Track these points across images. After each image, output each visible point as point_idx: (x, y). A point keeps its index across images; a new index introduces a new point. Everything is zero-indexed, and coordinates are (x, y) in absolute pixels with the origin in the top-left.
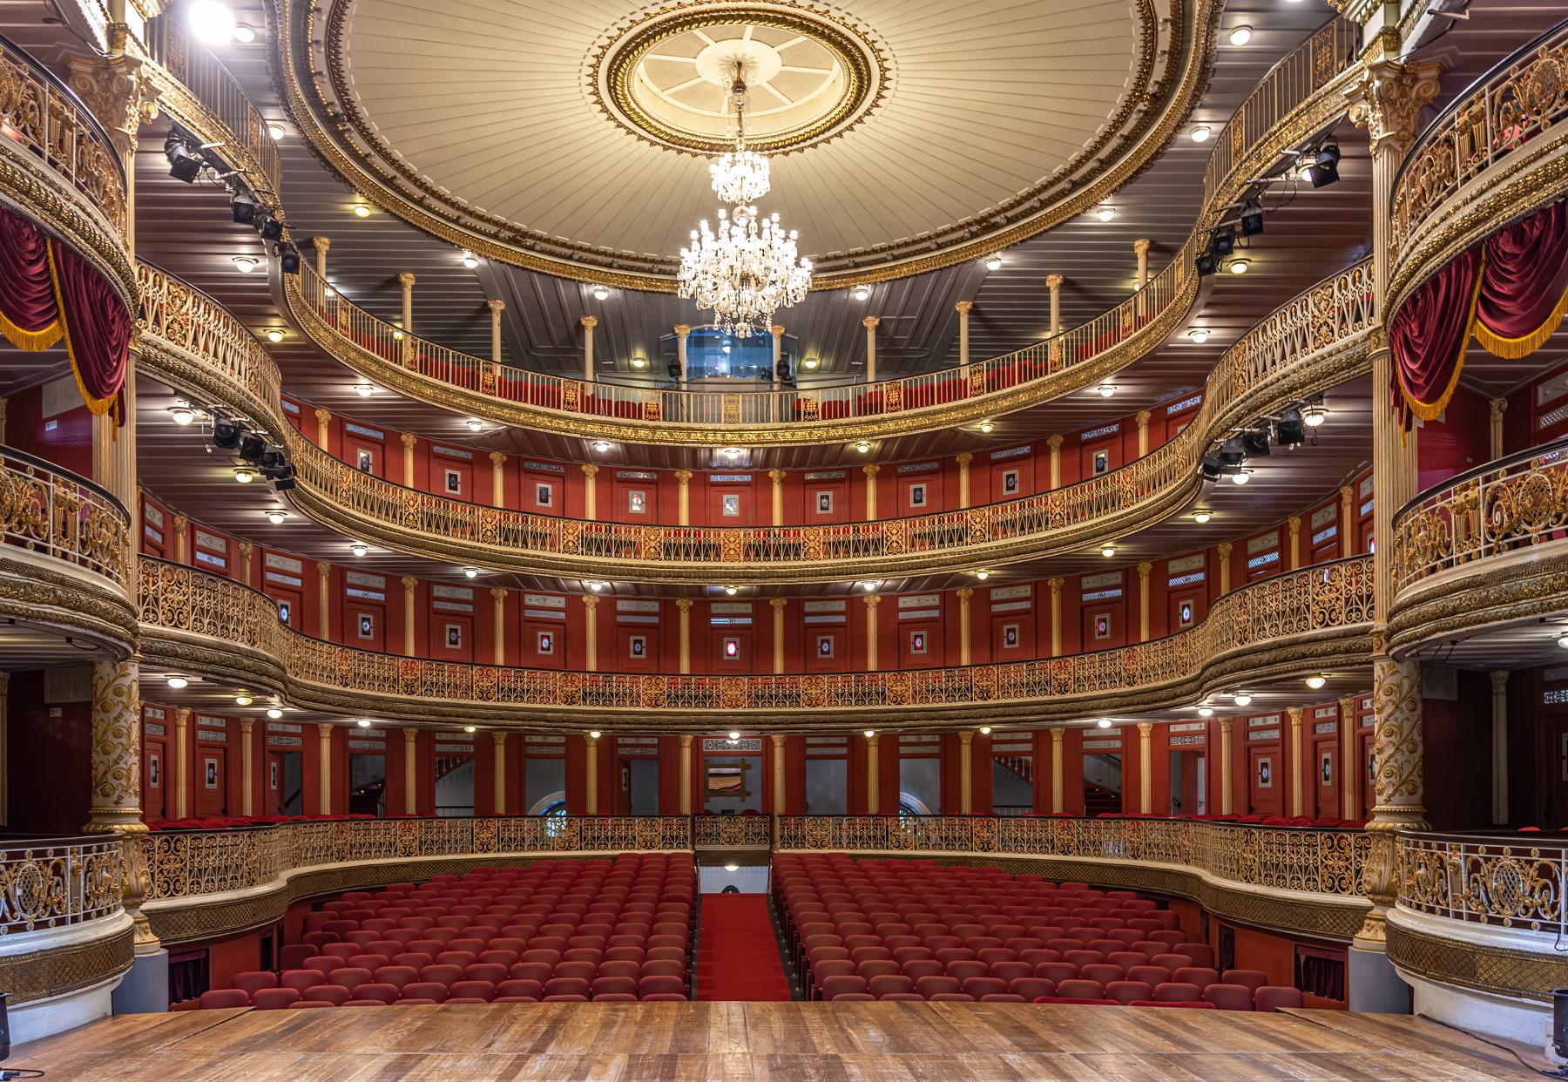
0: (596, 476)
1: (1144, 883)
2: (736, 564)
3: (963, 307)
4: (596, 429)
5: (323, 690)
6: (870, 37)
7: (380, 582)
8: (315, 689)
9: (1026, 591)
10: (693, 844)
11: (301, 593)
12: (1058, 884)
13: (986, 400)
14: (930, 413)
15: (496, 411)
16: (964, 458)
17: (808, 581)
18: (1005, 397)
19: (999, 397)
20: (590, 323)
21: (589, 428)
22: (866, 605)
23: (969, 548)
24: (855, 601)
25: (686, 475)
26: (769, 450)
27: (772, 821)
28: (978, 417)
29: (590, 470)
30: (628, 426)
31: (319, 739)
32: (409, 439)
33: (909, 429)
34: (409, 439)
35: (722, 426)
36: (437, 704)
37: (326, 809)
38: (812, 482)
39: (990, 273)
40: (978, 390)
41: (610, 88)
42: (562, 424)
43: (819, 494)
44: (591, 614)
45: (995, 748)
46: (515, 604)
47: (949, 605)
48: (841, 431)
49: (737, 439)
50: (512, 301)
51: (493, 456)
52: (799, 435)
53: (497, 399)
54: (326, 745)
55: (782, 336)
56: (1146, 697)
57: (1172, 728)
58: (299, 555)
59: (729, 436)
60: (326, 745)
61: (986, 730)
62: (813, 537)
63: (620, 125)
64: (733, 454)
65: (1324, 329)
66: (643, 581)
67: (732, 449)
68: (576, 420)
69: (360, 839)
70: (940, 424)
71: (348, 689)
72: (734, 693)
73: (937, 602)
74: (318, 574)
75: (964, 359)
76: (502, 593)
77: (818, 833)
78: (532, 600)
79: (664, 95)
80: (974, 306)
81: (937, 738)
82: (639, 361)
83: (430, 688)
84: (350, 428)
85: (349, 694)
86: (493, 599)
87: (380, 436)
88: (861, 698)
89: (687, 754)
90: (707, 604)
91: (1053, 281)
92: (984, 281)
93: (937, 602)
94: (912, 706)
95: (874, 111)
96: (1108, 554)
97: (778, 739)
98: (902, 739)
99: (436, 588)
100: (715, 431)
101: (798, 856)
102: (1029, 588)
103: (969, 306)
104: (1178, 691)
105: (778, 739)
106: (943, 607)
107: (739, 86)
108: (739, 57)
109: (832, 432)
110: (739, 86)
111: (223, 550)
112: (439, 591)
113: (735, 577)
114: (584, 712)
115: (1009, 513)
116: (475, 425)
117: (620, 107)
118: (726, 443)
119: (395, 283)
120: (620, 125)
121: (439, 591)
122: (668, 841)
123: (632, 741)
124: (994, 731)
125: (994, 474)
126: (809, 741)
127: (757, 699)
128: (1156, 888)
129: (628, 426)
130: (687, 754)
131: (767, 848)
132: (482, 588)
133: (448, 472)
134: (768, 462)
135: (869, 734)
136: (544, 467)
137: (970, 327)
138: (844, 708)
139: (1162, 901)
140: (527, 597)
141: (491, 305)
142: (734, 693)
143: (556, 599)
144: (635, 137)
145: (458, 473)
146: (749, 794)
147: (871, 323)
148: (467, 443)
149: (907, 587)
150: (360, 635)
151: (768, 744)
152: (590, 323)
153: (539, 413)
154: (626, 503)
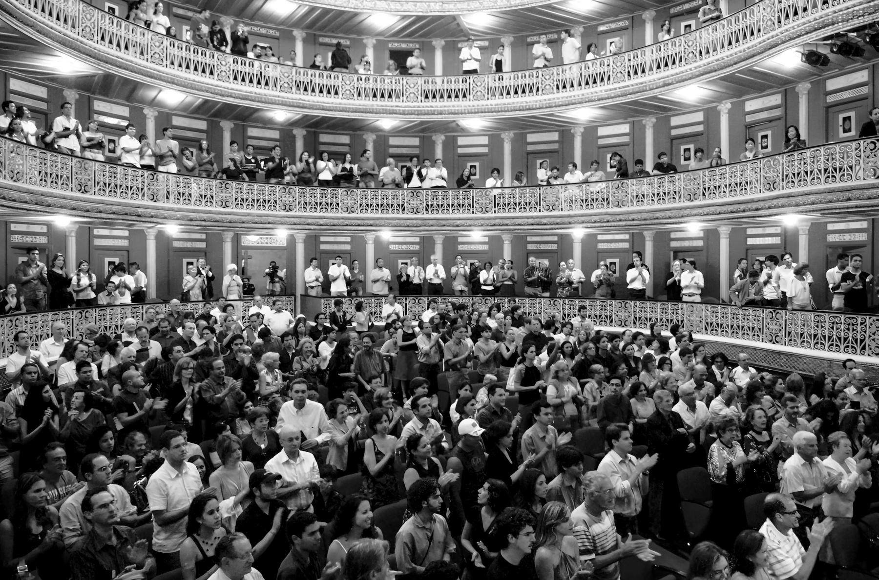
9: (625, 128)
94: (166, 205)
102: (702, 113)
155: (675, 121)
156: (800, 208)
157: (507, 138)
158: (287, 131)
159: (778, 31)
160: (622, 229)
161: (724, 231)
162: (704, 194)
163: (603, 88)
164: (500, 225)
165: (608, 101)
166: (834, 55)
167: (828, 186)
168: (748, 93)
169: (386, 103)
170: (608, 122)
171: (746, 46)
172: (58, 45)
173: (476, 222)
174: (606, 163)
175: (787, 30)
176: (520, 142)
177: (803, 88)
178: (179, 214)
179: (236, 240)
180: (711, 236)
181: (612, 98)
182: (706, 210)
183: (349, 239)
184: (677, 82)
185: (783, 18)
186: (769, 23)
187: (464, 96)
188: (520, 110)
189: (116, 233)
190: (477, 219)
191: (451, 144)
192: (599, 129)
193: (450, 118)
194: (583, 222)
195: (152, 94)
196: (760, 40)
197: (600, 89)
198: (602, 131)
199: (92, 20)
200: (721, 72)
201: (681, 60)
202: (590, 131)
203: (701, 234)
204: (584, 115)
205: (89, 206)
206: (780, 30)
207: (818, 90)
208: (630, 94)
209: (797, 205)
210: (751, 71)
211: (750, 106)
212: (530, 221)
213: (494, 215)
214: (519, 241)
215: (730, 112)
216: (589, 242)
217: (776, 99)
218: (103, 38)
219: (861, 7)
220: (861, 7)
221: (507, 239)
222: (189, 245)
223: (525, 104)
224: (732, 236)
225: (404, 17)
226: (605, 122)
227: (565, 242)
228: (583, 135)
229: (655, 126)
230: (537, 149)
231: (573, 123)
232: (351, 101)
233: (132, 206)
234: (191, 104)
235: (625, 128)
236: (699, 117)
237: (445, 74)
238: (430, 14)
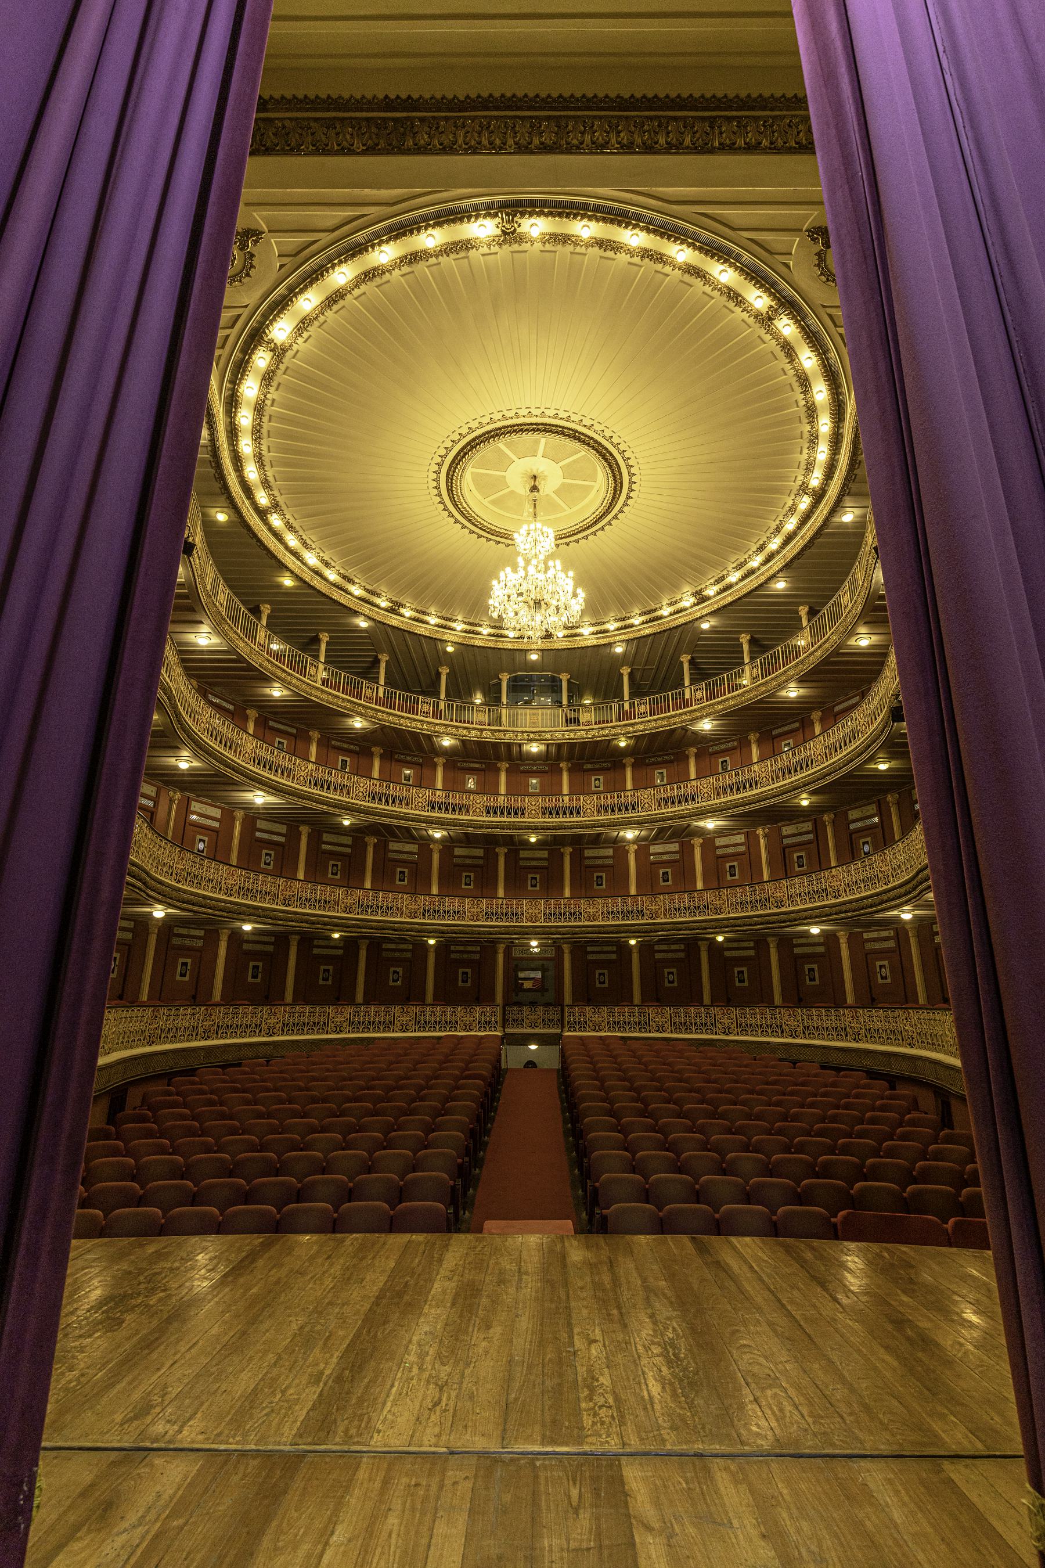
0: (444, 765)
1: (868, 1063)
2: (536, 820)
3: (685, 659)
4: (442, 729)
5: (204, 897)
6: (622, 447)
7: (283, 829)
8: (192, 894)
9: (741, 839)
10: (504, 1027)
11: (217, 832)
12: (794, 1063)
13: (706, 706)
14: (667, 717)
15: (371, 713)
17: (587, 831)
18: (719, 703)
19: (715, 704)
20: (444, 671)
21: (437, 728)
22: (627, 852)
24: (619, 844)
25: (504, 765)
26: (559, 746)
27: (563, 1011)
28: (701, 718)
29: (440, 761)
30: (464, 728)
31: (218, 940)
32: (315, 735)
33: (654, 728)
34: (315, 735)
35: (528, 729)
36: (308, 915)
37: (144, 997)
39: (703, 632)
40: (699, 701)
41: (448, 490)
42: (419, 725)
43: (593, 778)
44: (436, 857)
45: (727, 954)
46: (381, 848)
47: (686, 850)
48: (607, 732)
49: (537, 737)
50: (393, 653)
51: (373, 749)
52: (579, 735)
53: (374, 706)
54: (223, 947)
55: (569, 681)
56: (853, 906)
57: (865, 936)
58: (219, 804)
59: (532, 736)
60: (223, 947)
61: (720, 939)
62: (588, 802)
63: (457, 521)
64: (534, 748)
66: (471, 831)
67: (534, 744)
68: (428, 723)
69: (228, 1021)
70: (675, 723)
71: (232, 899)
72: (596, 1019)
73: (677, 849)
74: (233, 819)
75: (687, 682)
76: (371, 840)
77: (596, 1019)
78: (394, 846)
79: (485, 502)
80: (692, 658)
81: (682, 947)
82: (478, 699)
83: (305, 901)
84: (271, 723)
85: (231, 902)
86: (366, 845)
87: (295, 731)
88: (625, 915)
89: (500, 958)
90: (517, 851)
91: (744, 639)
92: (699, 639)
93: (677, 849)
95: (625, 509)
96: (805, 803)
97: (566, 948)
98: (656, 947)
99: (325, 835)
100: (522, 732)
101: (581, 1038)
103: (689, 657)
104: (885, 897)
105: (566, 948)
106: (682, 851)
107: (534, 489)
108: (535, 473)
109: (602, 732)
110: (534, 489)
111: (153, 794)
112: (326, 837)
113: (534, 828)
114: (422, 924)
115: (727, 779)
116: (358, 723)
117: (455, 505)
118: (531, 740)
119: (316, 640)
120: (457, 521)
121: (326, 837)
122: (483, 1025)
123: (461, 948)
124: (726, 940)
125: (713, 760)
126: (589, 949)
127: (548, 916)
128: (882, 1069)
129: (464, 728)
130: (500, 958)
131: (559, 1031)
132: (358, 832)
133: (341, 758)
134: (559, 757)
135: (633, 942)
136: (409, 758)
137: (691, 674)
138: (613, 923)
139: (893, 1081)
140: (391, 844)
141: (380, 657)
143: (412, 846)
144: (467, 531)
145: (348, 759)
146: (547, 990)
147: (625, 671)
148: (352, 739)
149: (656, 837)
150: (206, 839)
151: (559, 950)
152: (444, 671)
153: (403, 717)
154: (464, 783)
211: (787, 830)
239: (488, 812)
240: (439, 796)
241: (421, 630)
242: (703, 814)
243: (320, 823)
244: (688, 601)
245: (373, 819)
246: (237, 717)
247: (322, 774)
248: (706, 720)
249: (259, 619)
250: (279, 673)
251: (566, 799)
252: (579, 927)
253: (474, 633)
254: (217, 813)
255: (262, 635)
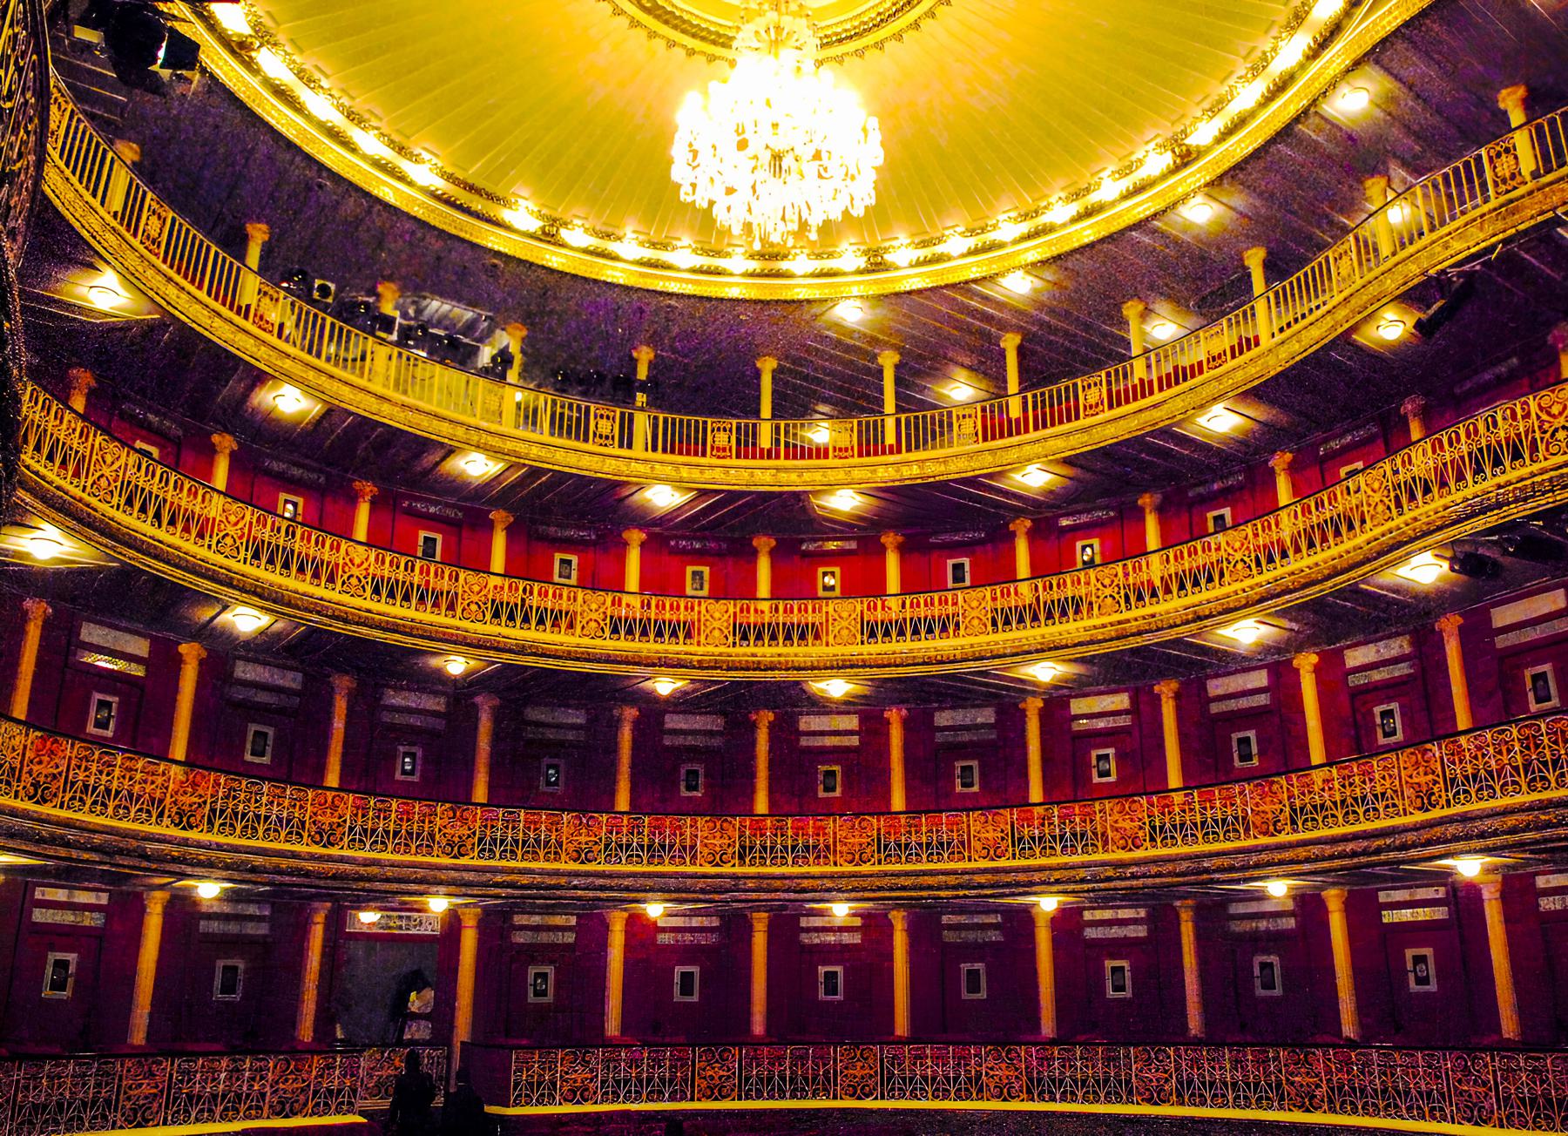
16: (1022, 526)
23: (831, 650)
29: (635, 537)
38: (684, 552)
65: (1380, 508)
72: (580, 1075)
102: (1264, 673)
105: (898, 920)
133: (422, 534)
142: (580, 1075)
155: (1216, 687)
156: (1490, 842)
157: (894, 716)
158: (462, 692)
159: (1399, 521)
160: (1131, 897)
161: (1334, 899)
162: (1293, 822)
163: (1080, 624)
164: (891, 889)
165: (1091, 647)
166: (1509, 559)
167: (1535, 796)
168: (1346, 636)
169: (669, 648)
170: (1087, 689)
171: (1342, 548)
172: (39, 505)
173: (843, 883)
174: (1089, 766)
175: (1415, 519)
176: (918, 728)
177: (1449, 626)
178: (228, 857)
179: (337, 922)
180: (1309, 906)
181: (1100, 642)
182: (1302, 853)
183: (573, 921)
184: (1220, 614)
185: (1404, 501)
186: (1380, 508)
187: (817, 637)
188: (924, 663)
189: (83, 897)
190: (842, 876)
191: (785, 732)
192: (1073, 701)
193: (792, 676)
194: (1057, 882)
195: (205, 614)
196: (1365, 537)
197: (1071, 629)
198: (1078, 706)
199: (115, 467)
200: (1301, 593)
201: (1363, 521)
202: (1056, 701)
203: (1290, 905)
204: (1045, 672)
205: (45, 830)
206: (1402, 518)
207: (1476, 634)
208: (1133, 635)
209: (1482, 835)
210: (1353, 592)
212: (951, 880)
213: (877, 868)
214: (924, 923)
215: (1317, 670)
216: (1066, 922)
217: (1399, 646)
218: (129, 502)
219: (1545, 477)
220: (1545, 477)
221: (898, 920)
222: (233, 928)
223: (933, 654)
224: (1349, 907)
225: (703, 493)
226: (1079, 687)
227: (1025, 918)
228: (1044, 715)
229: (1177, 696)
230: (955, 741)
231: (1024, 689)
232: (598, 642)
233: (134, 835)
234: (279, 636)
235: (1121, 701)
236: (1260, 679)
237: (775, 595)
238: (753, 489)
239: (615, 631)
240: (632, 603)
241: (555, 259)
242: (1230, 611)
243: (381, 664)
244: (1156, 161)
245: (506, 657)
246: (187, 456)
247: (390, 567)
248: (1218, 408)
249: (241, 256)
250: (287, 364)
251: (893, 603)
252: (557, 873)
253: (778, 275)
254: (141, 647)
255: (250, 286)
